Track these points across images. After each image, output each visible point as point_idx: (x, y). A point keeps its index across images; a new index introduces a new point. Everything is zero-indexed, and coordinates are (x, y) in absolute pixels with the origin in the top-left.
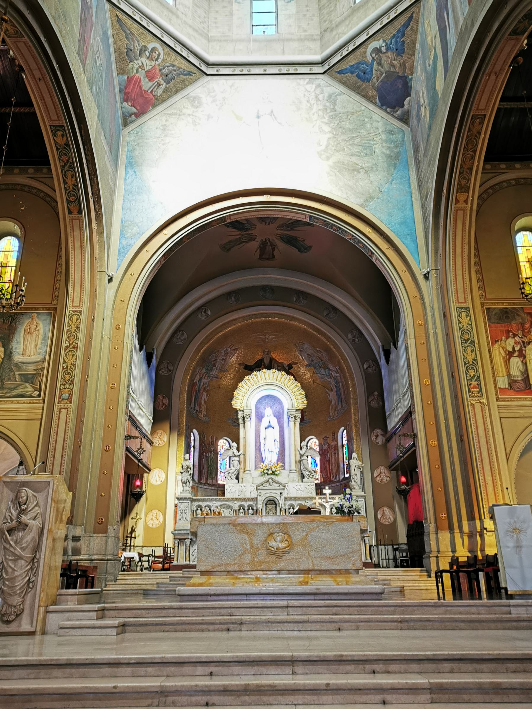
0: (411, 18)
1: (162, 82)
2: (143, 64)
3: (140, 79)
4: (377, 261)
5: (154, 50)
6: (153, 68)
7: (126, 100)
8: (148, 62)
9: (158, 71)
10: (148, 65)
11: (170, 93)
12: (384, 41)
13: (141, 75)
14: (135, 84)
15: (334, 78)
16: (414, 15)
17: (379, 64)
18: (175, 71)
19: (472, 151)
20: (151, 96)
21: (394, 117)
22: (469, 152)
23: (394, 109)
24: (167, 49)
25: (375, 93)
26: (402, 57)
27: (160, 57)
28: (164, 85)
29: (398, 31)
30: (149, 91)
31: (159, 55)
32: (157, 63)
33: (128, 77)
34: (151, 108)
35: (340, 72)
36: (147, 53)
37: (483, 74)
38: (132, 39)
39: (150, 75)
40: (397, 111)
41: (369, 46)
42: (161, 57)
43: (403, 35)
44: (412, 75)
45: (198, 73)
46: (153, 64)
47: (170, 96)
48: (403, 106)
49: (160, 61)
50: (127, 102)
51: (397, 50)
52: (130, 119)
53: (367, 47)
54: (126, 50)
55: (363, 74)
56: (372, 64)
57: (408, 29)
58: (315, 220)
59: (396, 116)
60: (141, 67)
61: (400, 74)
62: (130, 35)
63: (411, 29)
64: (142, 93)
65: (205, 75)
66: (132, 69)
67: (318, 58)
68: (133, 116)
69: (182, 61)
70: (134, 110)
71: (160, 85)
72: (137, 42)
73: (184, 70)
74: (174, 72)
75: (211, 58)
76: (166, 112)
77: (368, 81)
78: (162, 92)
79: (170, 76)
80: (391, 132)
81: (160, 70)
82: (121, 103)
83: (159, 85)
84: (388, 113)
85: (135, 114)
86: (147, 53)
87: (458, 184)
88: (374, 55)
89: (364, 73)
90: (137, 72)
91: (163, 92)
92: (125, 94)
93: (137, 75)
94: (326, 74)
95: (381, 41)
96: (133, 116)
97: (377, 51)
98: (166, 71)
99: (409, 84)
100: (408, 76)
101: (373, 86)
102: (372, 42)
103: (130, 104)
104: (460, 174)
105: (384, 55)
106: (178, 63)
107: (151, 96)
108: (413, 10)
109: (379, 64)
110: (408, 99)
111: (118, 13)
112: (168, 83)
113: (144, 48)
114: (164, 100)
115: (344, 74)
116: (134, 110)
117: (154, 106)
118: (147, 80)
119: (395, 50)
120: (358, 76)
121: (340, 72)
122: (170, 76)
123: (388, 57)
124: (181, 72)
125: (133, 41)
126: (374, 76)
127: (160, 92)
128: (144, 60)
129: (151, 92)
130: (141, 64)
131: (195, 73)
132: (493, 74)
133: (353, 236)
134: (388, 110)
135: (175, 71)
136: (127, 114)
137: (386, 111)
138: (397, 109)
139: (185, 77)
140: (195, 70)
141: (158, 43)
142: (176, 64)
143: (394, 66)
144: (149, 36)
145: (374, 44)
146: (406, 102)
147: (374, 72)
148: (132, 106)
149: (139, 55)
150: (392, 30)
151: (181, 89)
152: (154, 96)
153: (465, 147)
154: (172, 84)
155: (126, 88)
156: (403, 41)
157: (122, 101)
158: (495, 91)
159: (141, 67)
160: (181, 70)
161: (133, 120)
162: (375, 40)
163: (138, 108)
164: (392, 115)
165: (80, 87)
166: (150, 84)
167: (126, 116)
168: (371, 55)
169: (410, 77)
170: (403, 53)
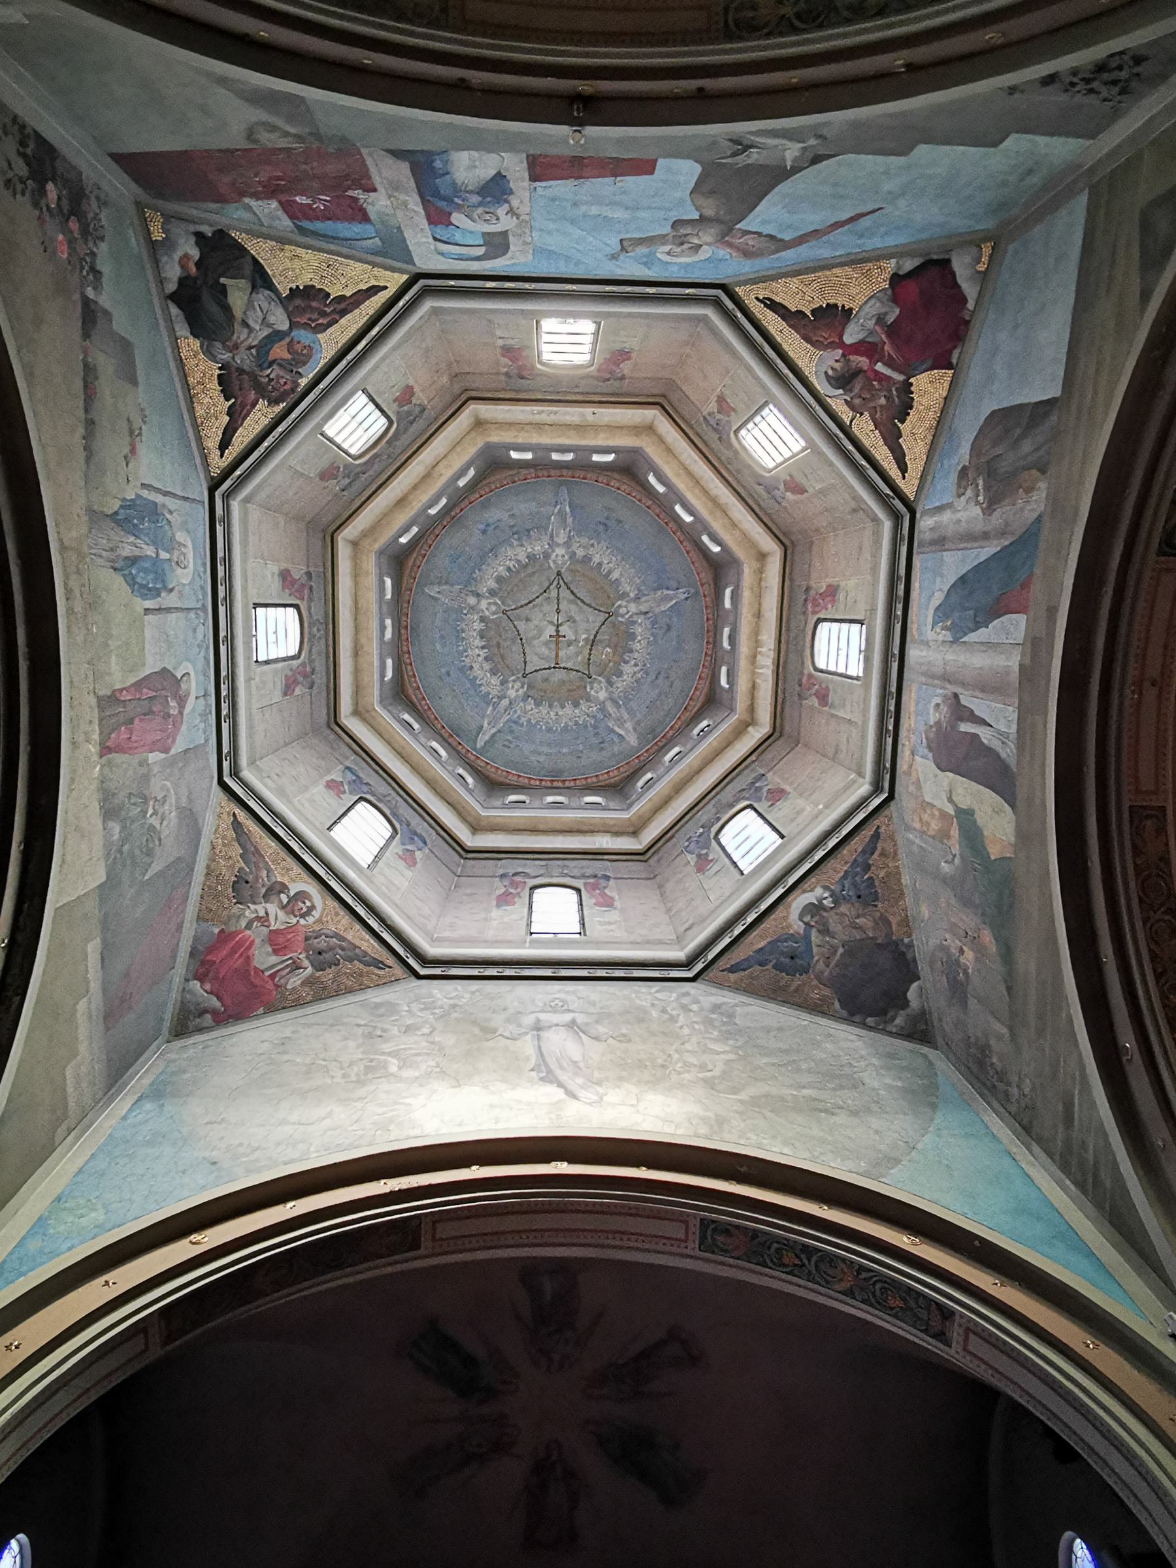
0: (876, 836)
1: (306, 963)
2: (267, 913)
3: (253, 941)
4: (974, 1343)
5: (302, 896)
6: (291, 929)
7: (201, 978)
8: (281, 914)
9: (301, 938)
10: (278, 917)
11: (320, 993)
12: (826, 888)
13: (258, 934)
14: (233, 951)
15: (719, 984)
16: (882, 830)
17: (825, 931)
18: (343, 949)
19: (1165, 913)
20: (270, 986)
21: (890, 1034)
22: (1158, 915)
23: (886, 1014)
24: (333, 904)
25: (827, 992)
26: (876, 906)
27: (314, 913)
28: (310, 970)
29: (852, 864)
30: (267, 973)
31: (313, 907)
32: (302, 921)
33: (222, 931)
34: (261, 1010)
35: (732, 969)
36: (284, 898)
37: (1121, 690)
38: (256, 864)
39: (278, 942)
40: (893, 1019)
41: (794, 905)
42: (316, 914)
43: (867, 867)
44: (910, 936)
45: (398, 970)
46: (294, 921)
47: (318, 998)
48: (906, 1004)
49: (311, 920)
50: (202, 981)
51: (859, 897)
52: (198, 1020)
53: (790, 906)
54: (234, 879)
55: (788, 960)
56: (807, 937)
57: (875, 856)
58: (720, 1239)
59: (894, 1030)
60: (264, 920)
61: (879, 941)
62: (250, 853)
63: (882, 855)
64: (246, 972)
65: (413, 978)
66: (239, 917)
67: (680, 955)
68: (208, 1016)
69: (364, 933)
70: (215, 1002)
71: (298, 968)
72: (265, 872)
73: (365, 954)
74: (340, 951)
75: (432, 950)
76: (301, 1021)
77: (805, 970)
78: (299, 982)
79: (327, 956)
80: (891, 1056)
81: (307, 939)
82: (187, 980)
83: (296, 966)
84: (870, 1028)
85: (215, 1013)
86: (284, 898)
87: (1165, 1006)
88: (807, 919)
89: (792, 958)
90: (249, 926)
91: (303, 984)
92: (203, 963)
93: (248, 932)
94: (699, 980)
95: (819, 891)
96: (208, 1016)
97: (815, 909)
98: (321, 943)
99: (909, 956)
100: (902, 940)
101: (819, 977)
102: (799, 896)
103: (208, 987)
104: (1158, 977)
105: (832, 913)
106: (354, 937)
107: (270, 986)
108: (877, 822)
109: (825, 931)
110: (915, 984)
111: (237, 811)
112: (319, 967)
113: (278, 887)
114: (299, 1003)
115: (744, 970)
116: (215, 1002)
117: (271, 1009)
118: (270, 949)
119: (854, 898)
120: (779, 967)
121: (732, 969)
122: (327, 956)
123: (843, 915)
124: (357, 955)
125: (258, 868)
126: (816, 958)
127: (294, 982)
128: (272, 908)
129: (272, 976)
130: (262, 913)
131: (390, 967)
132: (1147, 684)
133: (862, 1268)
134: (870, 1021)
135: (343, 949)
136: (192, 1008)
137: (864, 1025)
138: (891, 1013)
139: (366, 969)
140: (390, 960)
141: (314, 887)
142: (349, 937)
143: (860, 928)
144: (297, 869)
145: (801, 900)
146: (912, 993)
147: (815, 950)
148: (211, 993)
149: (263, 897)
150: (838, 868)
151: (350, 991)
152: (277, 986)
153: (1141, 901)
154: (329, 974)
155: (211, 949)
156: (870, 878)
157: (190, 976)
158: (1166, 730)
159: (264, 920)
160: (357, 950)
161: (205, 1024)
162: (804, 892)
163: (229, 1002)
164: (884, 1030)
165: (30, 375)
166: (274, 959)
167: (190, 1012)
168: (802, 921)
169: (906, 940)
170: (876, 899)
